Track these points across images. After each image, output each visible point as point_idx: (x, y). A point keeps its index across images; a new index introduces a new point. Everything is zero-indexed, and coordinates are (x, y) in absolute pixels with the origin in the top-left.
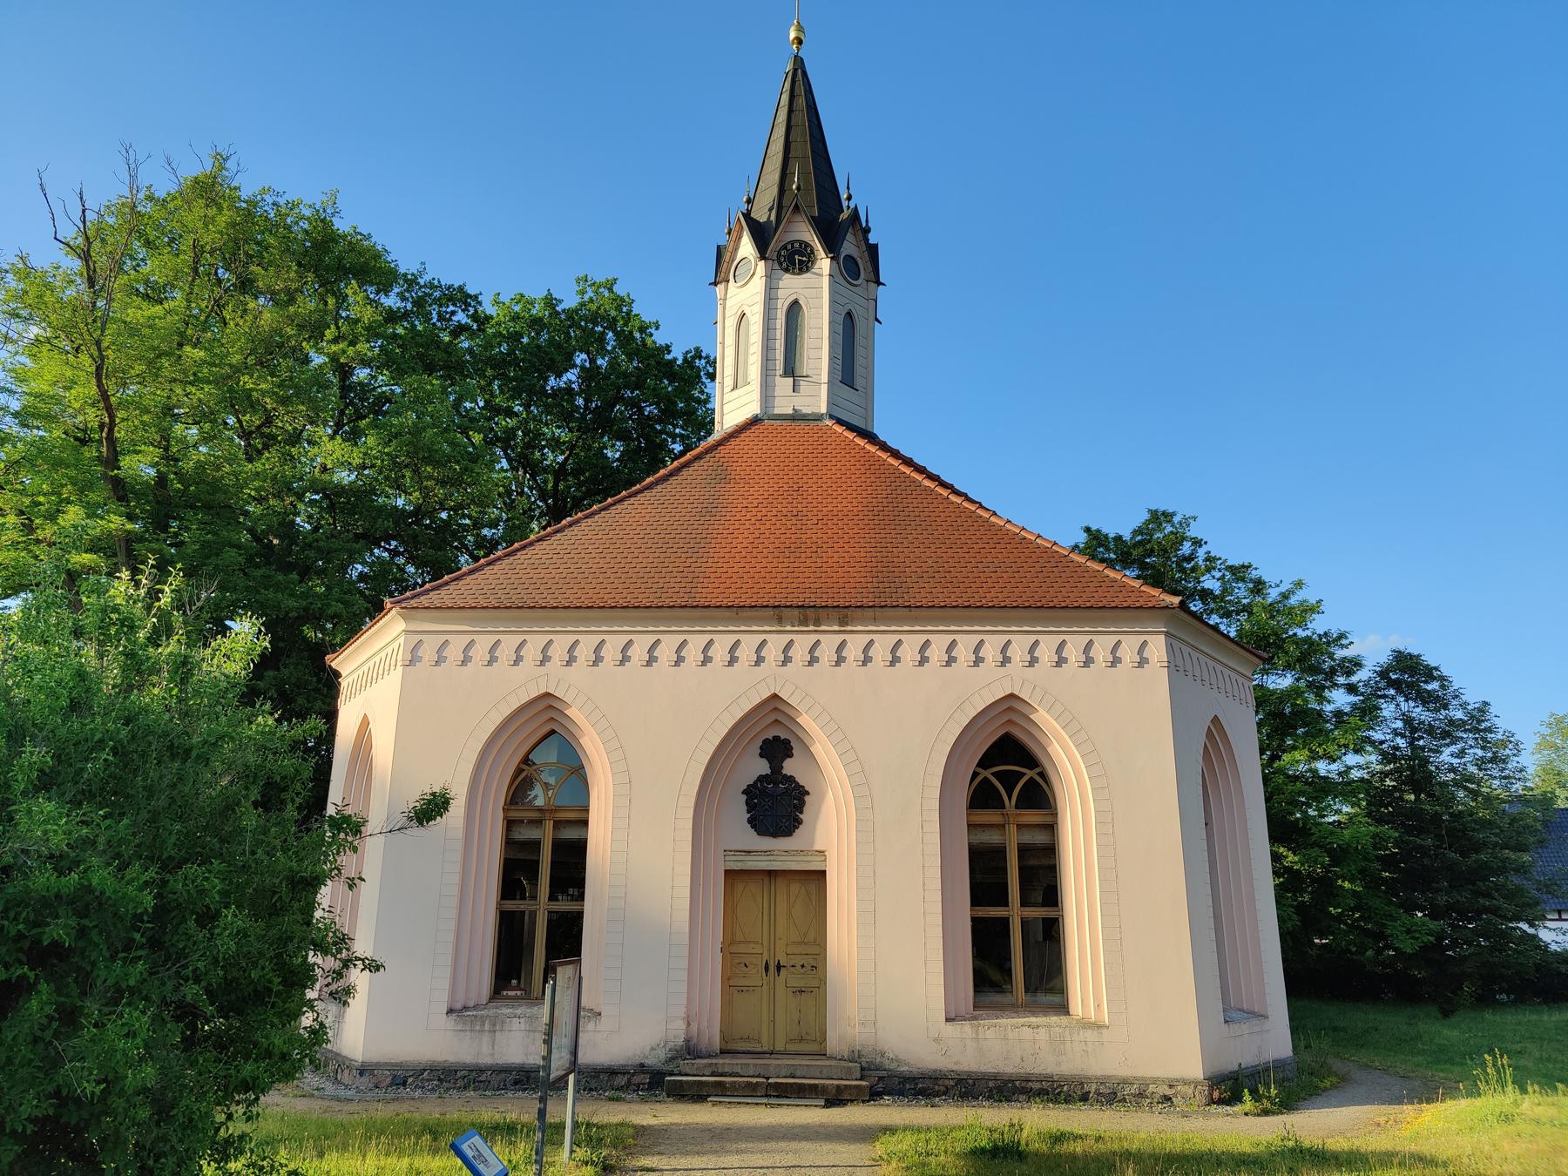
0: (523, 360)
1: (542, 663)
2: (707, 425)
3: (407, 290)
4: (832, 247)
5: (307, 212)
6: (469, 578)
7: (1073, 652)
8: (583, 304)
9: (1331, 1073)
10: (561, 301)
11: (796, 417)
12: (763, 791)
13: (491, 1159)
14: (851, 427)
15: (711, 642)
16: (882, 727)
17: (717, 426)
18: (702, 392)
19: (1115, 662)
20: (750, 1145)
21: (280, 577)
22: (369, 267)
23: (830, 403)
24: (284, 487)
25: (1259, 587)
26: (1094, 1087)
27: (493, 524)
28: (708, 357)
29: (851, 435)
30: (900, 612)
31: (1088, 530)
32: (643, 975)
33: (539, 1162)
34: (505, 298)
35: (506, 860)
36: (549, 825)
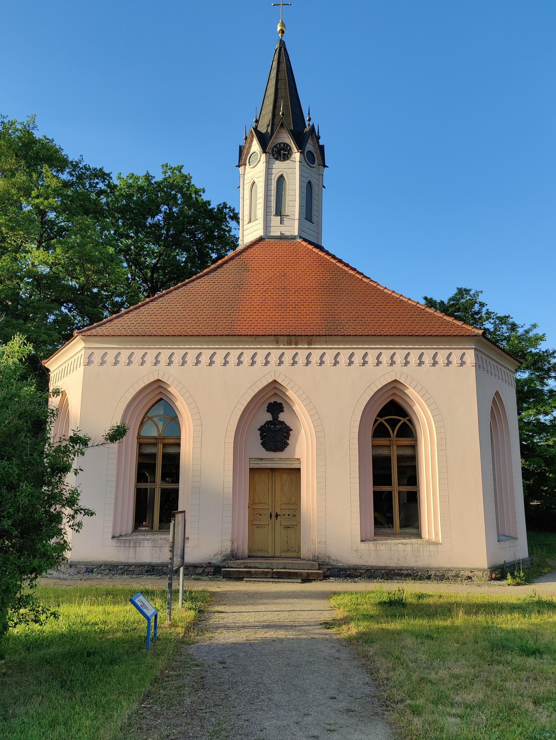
0: (135, 209)
1: (155, 364)
2: (233, 244)
3: (73, 170)
4: (301, 146)
5: (19, 127)
6: (116, 320)
7: (427, 359)
8: (165, 179)
9: (547, 566)
10: (154, 177)
11: (282, 237)
12: (269, 429)
13: (149, 606)
14: (310, 243)
15: (242, 354)
16: (330, 396)
17: (240, 242)
18: (227, 226)
19: (449, 363)
20: (268, 601)
21: (14, 321)
22: (51, 157)
23: (300, 230)
24: (13, 275)
25: (514, 327)
26: (433, 573)
27: (120, 295)
28: (230, 207)
29: (310, 247)
30: (339, 338)
31: (426, 298)
32: (210, 522)
33: (169, 608)
34: (124, 176)
35: (139, 463)
36: (160, 446)
